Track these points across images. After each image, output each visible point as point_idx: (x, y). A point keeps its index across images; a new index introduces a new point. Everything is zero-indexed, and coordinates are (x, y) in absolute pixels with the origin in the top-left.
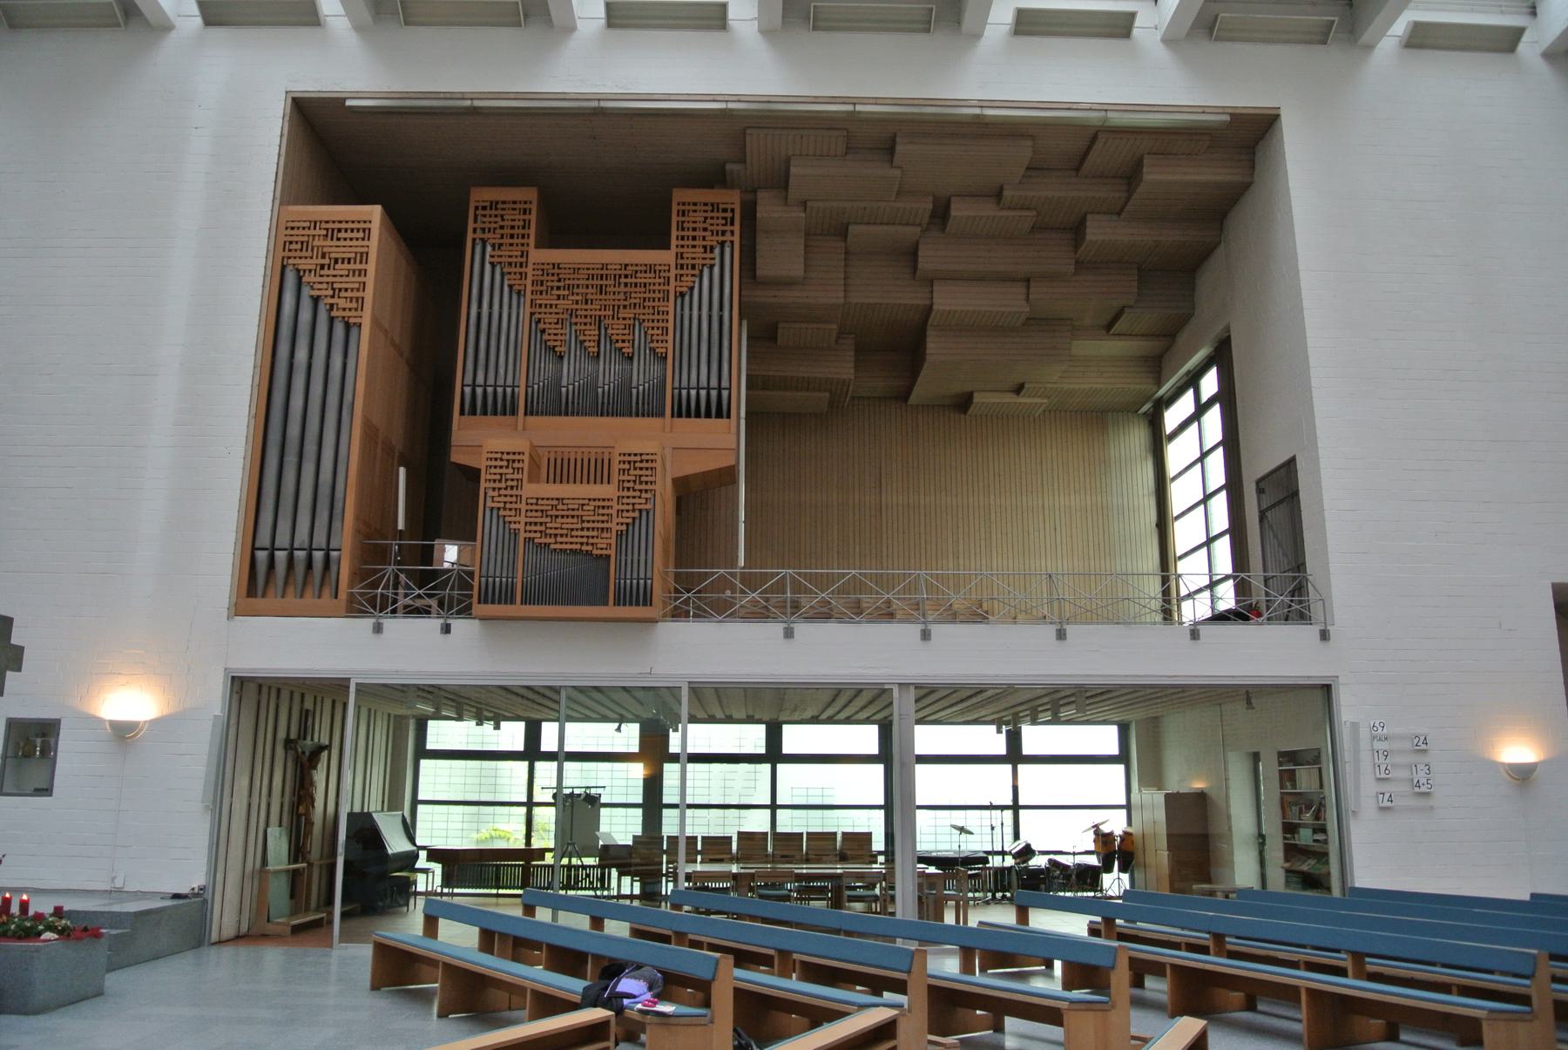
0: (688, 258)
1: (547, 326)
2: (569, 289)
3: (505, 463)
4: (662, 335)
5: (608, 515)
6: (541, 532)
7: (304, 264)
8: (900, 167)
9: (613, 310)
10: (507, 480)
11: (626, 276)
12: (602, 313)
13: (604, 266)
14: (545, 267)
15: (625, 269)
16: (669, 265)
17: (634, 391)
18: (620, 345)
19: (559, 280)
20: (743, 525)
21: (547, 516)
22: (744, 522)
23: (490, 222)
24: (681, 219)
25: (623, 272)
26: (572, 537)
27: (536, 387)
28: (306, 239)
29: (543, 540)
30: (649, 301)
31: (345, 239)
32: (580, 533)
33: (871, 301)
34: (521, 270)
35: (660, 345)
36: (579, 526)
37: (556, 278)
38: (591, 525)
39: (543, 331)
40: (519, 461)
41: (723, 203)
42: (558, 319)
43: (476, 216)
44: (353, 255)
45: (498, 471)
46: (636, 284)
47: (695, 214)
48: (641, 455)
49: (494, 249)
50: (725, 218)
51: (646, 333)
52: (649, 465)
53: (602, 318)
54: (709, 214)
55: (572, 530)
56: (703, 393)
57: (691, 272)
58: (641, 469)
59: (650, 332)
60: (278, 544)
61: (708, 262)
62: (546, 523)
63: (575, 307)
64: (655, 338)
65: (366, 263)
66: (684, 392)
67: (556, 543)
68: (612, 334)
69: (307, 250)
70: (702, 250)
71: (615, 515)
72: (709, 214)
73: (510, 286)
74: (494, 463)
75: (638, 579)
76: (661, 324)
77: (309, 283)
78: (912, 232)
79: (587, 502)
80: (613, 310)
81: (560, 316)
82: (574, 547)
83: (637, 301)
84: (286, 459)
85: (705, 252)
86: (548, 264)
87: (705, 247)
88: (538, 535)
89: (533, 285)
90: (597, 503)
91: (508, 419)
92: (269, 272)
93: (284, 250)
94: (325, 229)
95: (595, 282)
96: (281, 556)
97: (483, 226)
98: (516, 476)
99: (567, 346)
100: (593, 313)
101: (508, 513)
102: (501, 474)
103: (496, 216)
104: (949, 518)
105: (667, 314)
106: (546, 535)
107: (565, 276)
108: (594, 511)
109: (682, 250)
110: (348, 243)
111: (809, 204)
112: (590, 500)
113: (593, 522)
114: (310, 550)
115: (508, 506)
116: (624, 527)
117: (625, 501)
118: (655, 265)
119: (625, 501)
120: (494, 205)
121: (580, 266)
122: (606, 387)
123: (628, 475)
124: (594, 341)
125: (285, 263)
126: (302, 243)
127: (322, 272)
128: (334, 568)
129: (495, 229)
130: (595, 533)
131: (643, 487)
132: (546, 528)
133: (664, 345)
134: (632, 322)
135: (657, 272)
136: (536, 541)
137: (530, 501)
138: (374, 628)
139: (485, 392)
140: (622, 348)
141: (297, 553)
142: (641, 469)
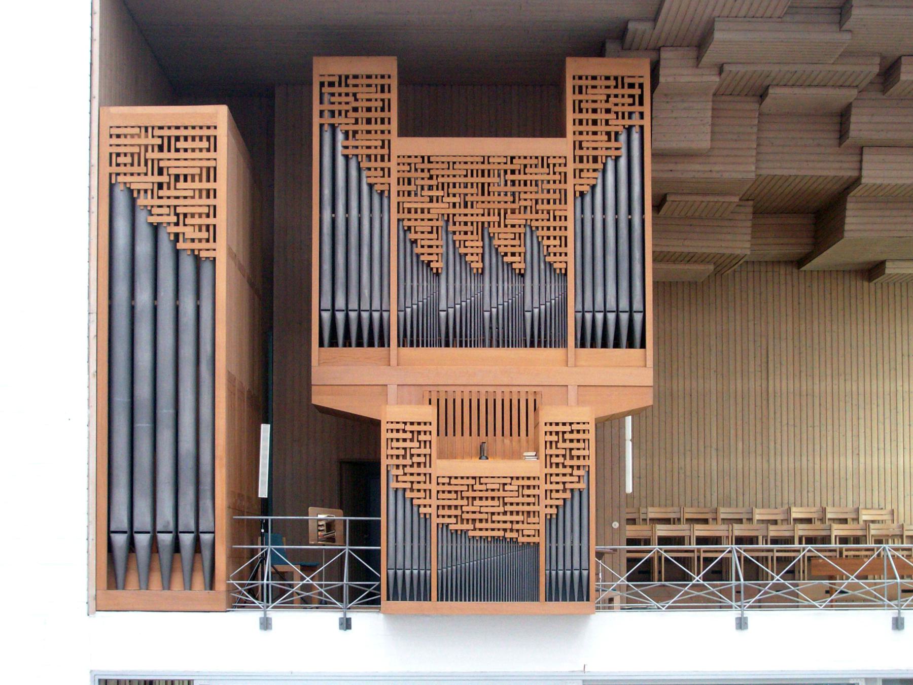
0: (588, 148)
1: (419, 236)
2: (443, 189)
3: (409, 435)
4: (560, 246)
5: (534, 496)
6: (456, 516)
7: (137, 183)
8: (850, 31)
9: (499, 215)
10: (412, 456)
11: (513, 172)
12: (486, 219)
13: (486, 159)
14: (412, 160)
15: (512, 163)
16: (565, 158)
17: (528, 315)
18: (508, 259)
19: (431, 178)
20: (631, 443)
21: (462, 498)
22: (632, 440)
23: (340, 103)
24: (579, 97)
25: (509, 167)
26: (493, 522)
27: (408, 310)
28: (136, 150)
29: (459, 527)
30: (543, 203)
31: (186, 150)
32: (502, 518)
33: (786, 172)
34: (382, 165)
35: (558, 258)
36: (501, 509)
37: (426, 175)
38: (514, 508)
39: (414, 242)
40: (425, 433)
41: (629, 77)
42: (432, 227)
43: (321, 95)
44: (197, 171)
45: (401, 444)
46: (525, 182)
47: (595, 91)
48: (571, 424)
49: (347, 138)
50: (632, 96)
51: (539, 243)
52: (581, 436)
53: (486, 225)
54: (613, 91)
55: (493, 514)
56: (611, 317)
57: (592, 166)
58: (571, 441)
59: (546, 242)
60: (137, 526)
61: (613, 153)
62: (462, 506)
63: (452, 211)
64: (551, 249)
65: (215, 181)
66: (588, 316)
67: (475, 529)
68: (499, 246)
69: (139, 165)
70: (606, 138)
71: (542, 496)
72: (613, 91)
73: (371, 186)
74: (395, 435)
75: (572, 570)
76: (557, 233)
77: (146, 206)
78: (849, 94)
79: (508, 481)
80: (499, 215)
81: (435, 223)
82: (496, 534)
83: (528, 203)
84: (137, 425)
85: (609, 140)
86: (416, 157)
87: (608, 134)
88: (453, 520)
89: (399, 184)
90: (521, 482)
91: (376, 351)
92: (94, 193)
93: (111, 165)
94: (159, 137)
95: (475, 180)
96: (142, 540)
97: (332, 107)
98: (422, 451)
99: (444, 260)
100: (475, 219)
101: (415, 494)
102: (405, 449)
103: (347, 95)
104: (849, 408)
105: (566, 220)
106: (462, 520)
107: (438, 172)
108: (518, 491)
109: (581, 138)
110: (189, 155)
111: (727, 68)
112: (512, 478)
113: (518, 504)
114: (177, 534)
115: (416, 486)
116: (554, 511)
117: (554, 479)
118: (548, 157)
119: (554, 479)
120: (343, 80)
121: (454, 159)
122: (494, 310)
123: (557, 448)
124: (477, 254)
125: (113, 181)
126: (132, 155)
127: (161, 193)
128: (206, 553)
129: (347, 111)
130: (520, 518)
131: (575, 462)
132: (463, 512)
133: (563, 258)
134: (522, 230)
135: (551, 166)
136: (451, 527)
137: (441, 480)
138: (261, 624)
139: (347, 317)
140: (512, 263)
141: (161, 536)
142: (571, 441)
